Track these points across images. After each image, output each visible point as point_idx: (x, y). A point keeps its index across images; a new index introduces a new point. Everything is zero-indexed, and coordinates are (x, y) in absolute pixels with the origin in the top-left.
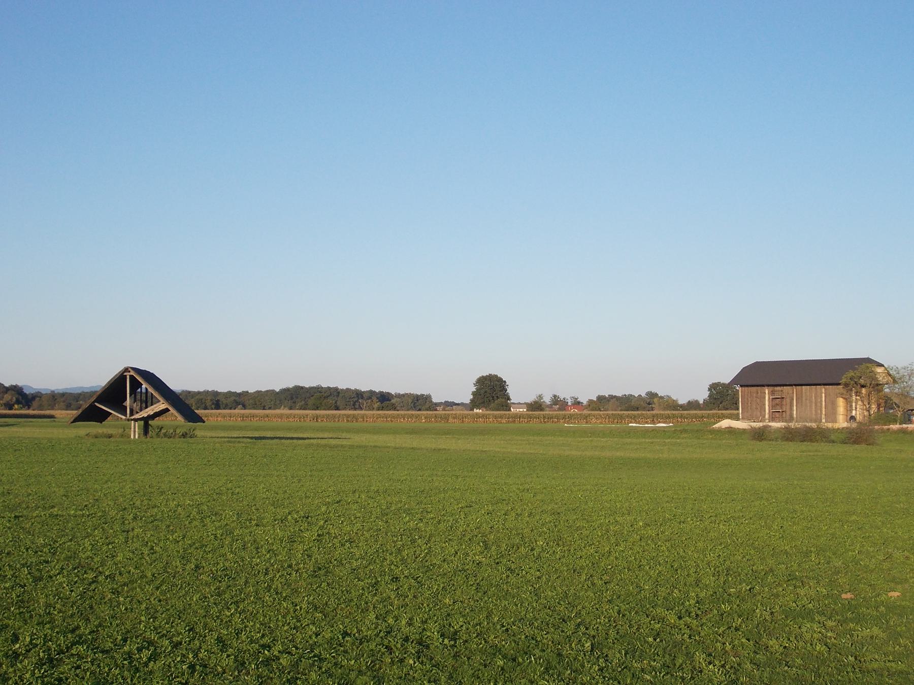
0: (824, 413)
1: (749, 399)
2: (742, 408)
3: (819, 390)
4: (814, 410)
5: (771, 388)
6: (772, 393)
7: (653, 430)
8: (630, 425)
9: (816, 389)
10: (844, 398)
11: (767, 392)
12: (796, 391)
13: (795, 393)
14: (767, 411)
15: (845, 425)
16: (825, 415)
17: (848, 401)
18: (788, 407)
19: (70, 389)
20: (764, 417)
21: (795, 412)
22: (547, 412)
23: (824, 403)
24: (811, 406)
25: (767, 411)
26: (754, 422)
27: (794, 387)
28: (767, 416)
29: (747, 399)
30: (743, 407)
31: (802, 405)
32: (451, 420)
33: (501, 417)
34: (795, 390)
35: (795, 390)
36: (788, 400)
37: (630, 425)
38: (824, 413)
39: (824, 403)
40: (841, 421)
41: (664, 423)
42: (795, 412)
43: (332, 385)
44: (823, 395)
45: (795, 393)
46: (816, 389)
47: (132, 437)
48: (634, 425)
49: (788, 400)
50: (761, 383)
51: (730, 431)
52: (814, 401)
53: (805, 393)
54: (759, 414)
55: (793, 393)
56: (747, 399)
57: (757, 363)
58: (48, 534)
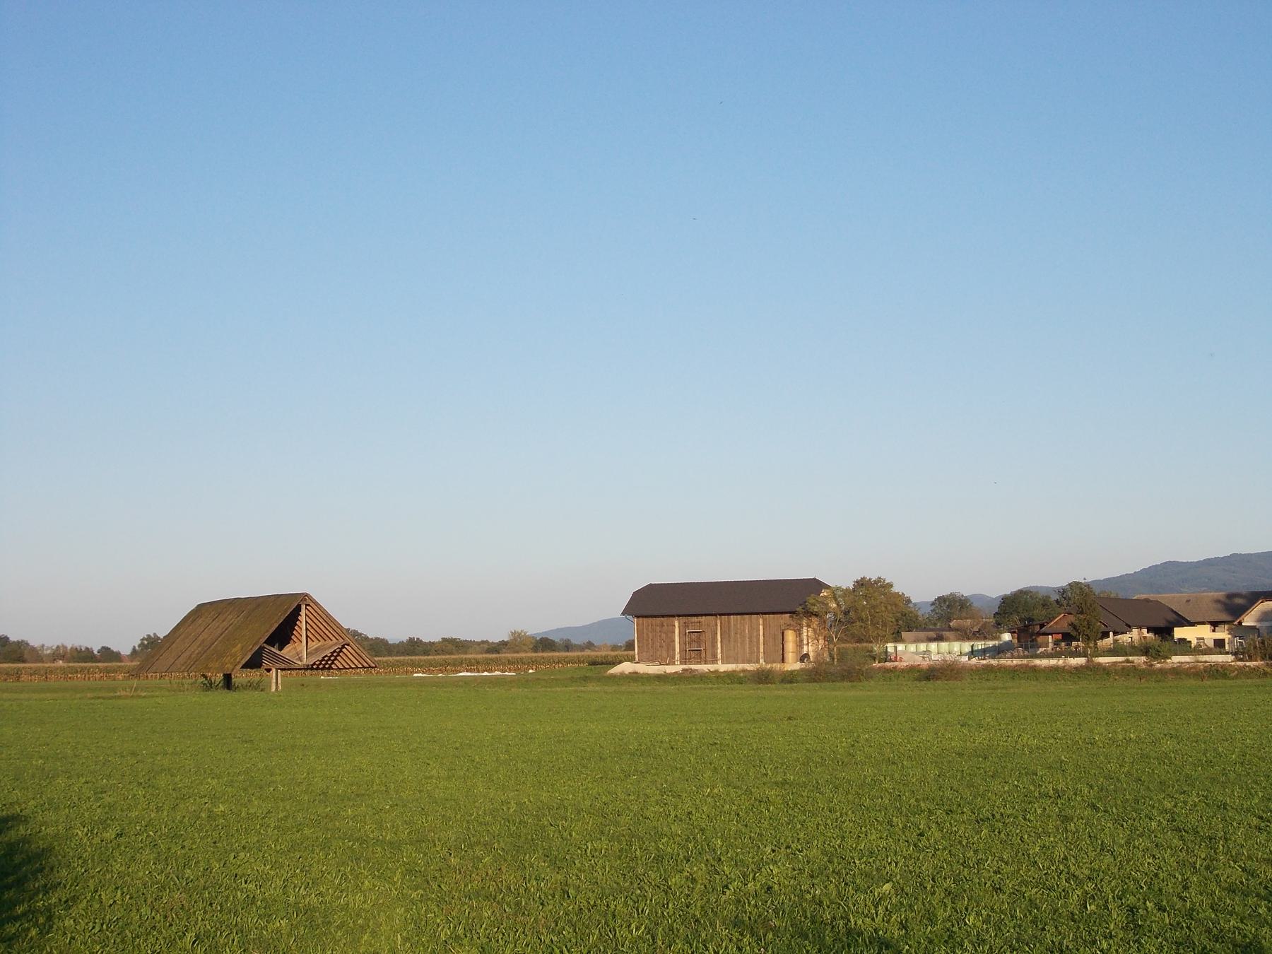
0: (762, 650)
1: (650, 634)
2: (638, 647)
3: (754, 621)
4: (748, 646)
5: (683, 619)
6: (686, 625)
7: (511, 682)
8: (415, 675)
9: (750, 619)
10: (795, 631)
11: (677, 624)
12: (721, 623)
13: (719, 624)
14: (677, 650)
15: (797, 666)
16: (764, 653)
17: (799, 633)
18: (709, 644)
19: (1108, 581)
20: (674, 658)
21: (719, 651)
22: (503, 655)
23: (761, 638)
24: (743, 642)
25: (677, 650)
26: (661, 665)
27: (718, 616)
28: (677, 657)
29: (647, 634)
30: (641, 645)
31: (729, 641)
32: (24, 677)
33: (115, 671)
34: (719, 622)
35: (719, 622)
36: (709, 635)
37: (415, 675)
38: (762, 650)
39: (761, 638)
40: (790, 661)
41: (423, 673)
42: (719, 651)
43: (1015, 589)
44: (761, 627)
45: (719, 624)
46: (750, 619)
47: (273, 689)
48: (420, 675)
49: (709, 635)
50: (749, 611)
51: (635, 677)
52: (747, 635)
53: (734, 625)
54: (664, 654)
55: (717, 625)
56: (647, 634)
57: (651, 587)
58: (147, 802)
